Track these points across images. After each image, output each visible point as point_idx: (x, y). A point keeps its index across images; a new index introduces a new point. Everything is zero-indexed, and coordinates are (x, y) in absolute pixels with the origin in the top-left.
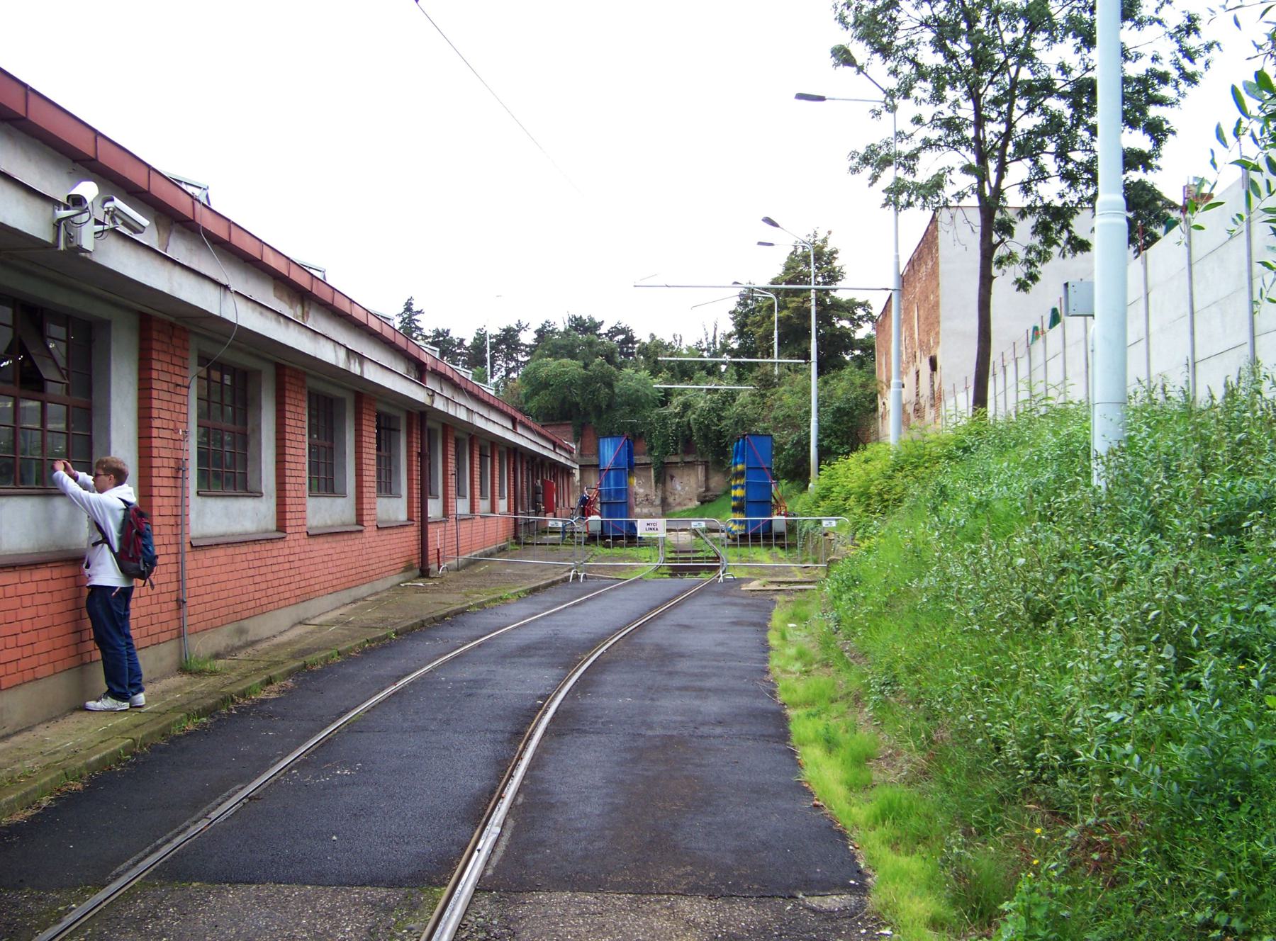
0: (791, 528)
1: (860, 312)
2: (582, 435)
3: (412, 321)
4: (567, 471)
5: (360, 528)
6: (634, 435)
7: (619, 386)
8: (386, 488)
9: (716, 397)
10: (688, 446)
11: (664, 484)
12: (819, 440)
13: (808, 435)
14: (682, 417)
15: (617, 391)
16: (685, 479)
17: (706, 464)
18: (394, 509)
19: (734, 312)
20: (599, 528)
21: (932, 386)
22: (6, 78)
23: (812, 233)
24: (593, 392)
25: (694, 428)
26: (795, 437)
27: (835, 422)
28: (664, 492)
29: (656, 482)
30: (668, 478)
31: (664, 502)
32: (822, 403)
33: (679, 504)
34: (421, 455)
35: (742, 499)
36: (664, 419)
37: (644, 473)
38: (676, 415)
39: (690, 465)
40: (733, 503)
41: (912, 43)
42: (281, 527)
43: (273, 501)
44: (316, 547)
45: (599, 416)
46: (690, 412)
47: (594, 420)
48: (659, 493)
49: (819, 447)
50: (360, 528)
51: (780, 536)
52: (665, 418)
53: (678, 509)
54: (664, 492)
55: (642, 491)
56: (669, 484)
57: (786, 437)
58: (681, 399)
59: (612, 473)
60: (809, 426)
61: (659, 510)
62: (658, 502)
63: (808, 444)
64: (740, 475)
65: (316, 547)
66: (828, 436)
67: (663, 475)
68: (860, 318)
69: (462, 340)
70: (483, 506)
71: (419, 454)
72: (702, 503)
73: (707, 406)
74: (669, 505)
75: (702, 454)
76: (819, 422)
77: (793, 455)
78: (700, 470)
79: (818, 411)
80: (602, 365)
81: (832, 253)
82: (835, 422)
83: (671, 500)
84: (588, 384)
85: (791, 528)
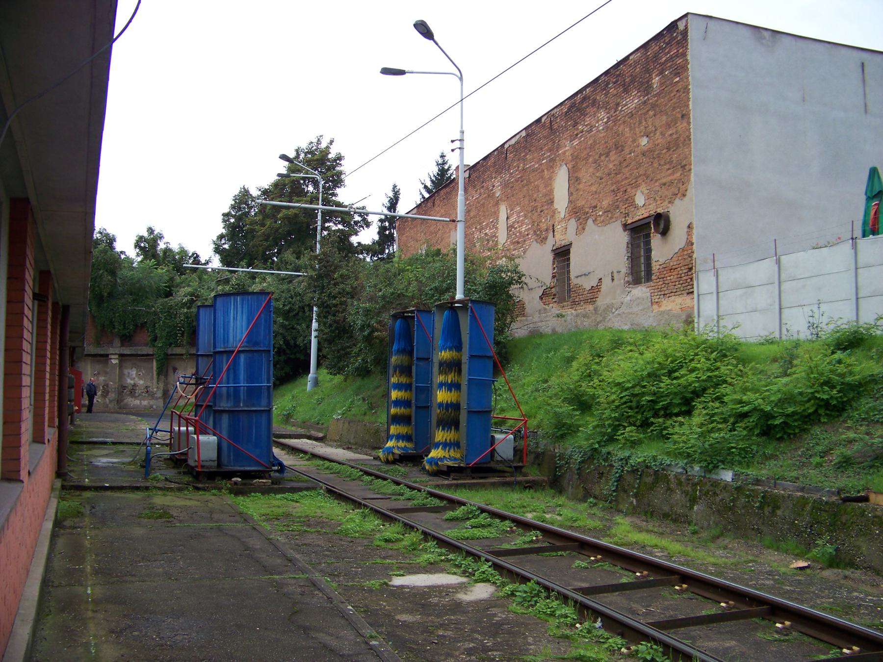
11: (166, 376)
20: (214, 455)
21: (215, 316)
23: (315, 140)
28: (166, 384)
29: (159, 374)
30: (171, 371)
31: (165, 393)
38: (184, 305)
48: (161, 385)
52: (171, 307)
54: (166, 384)
55: (141, 382)
59: (242, 357)
61: (161, 403)
62: (159, 394)
67: (165, 367)
68: (356, 223)
71: (36, 296)
81: (339, 158)
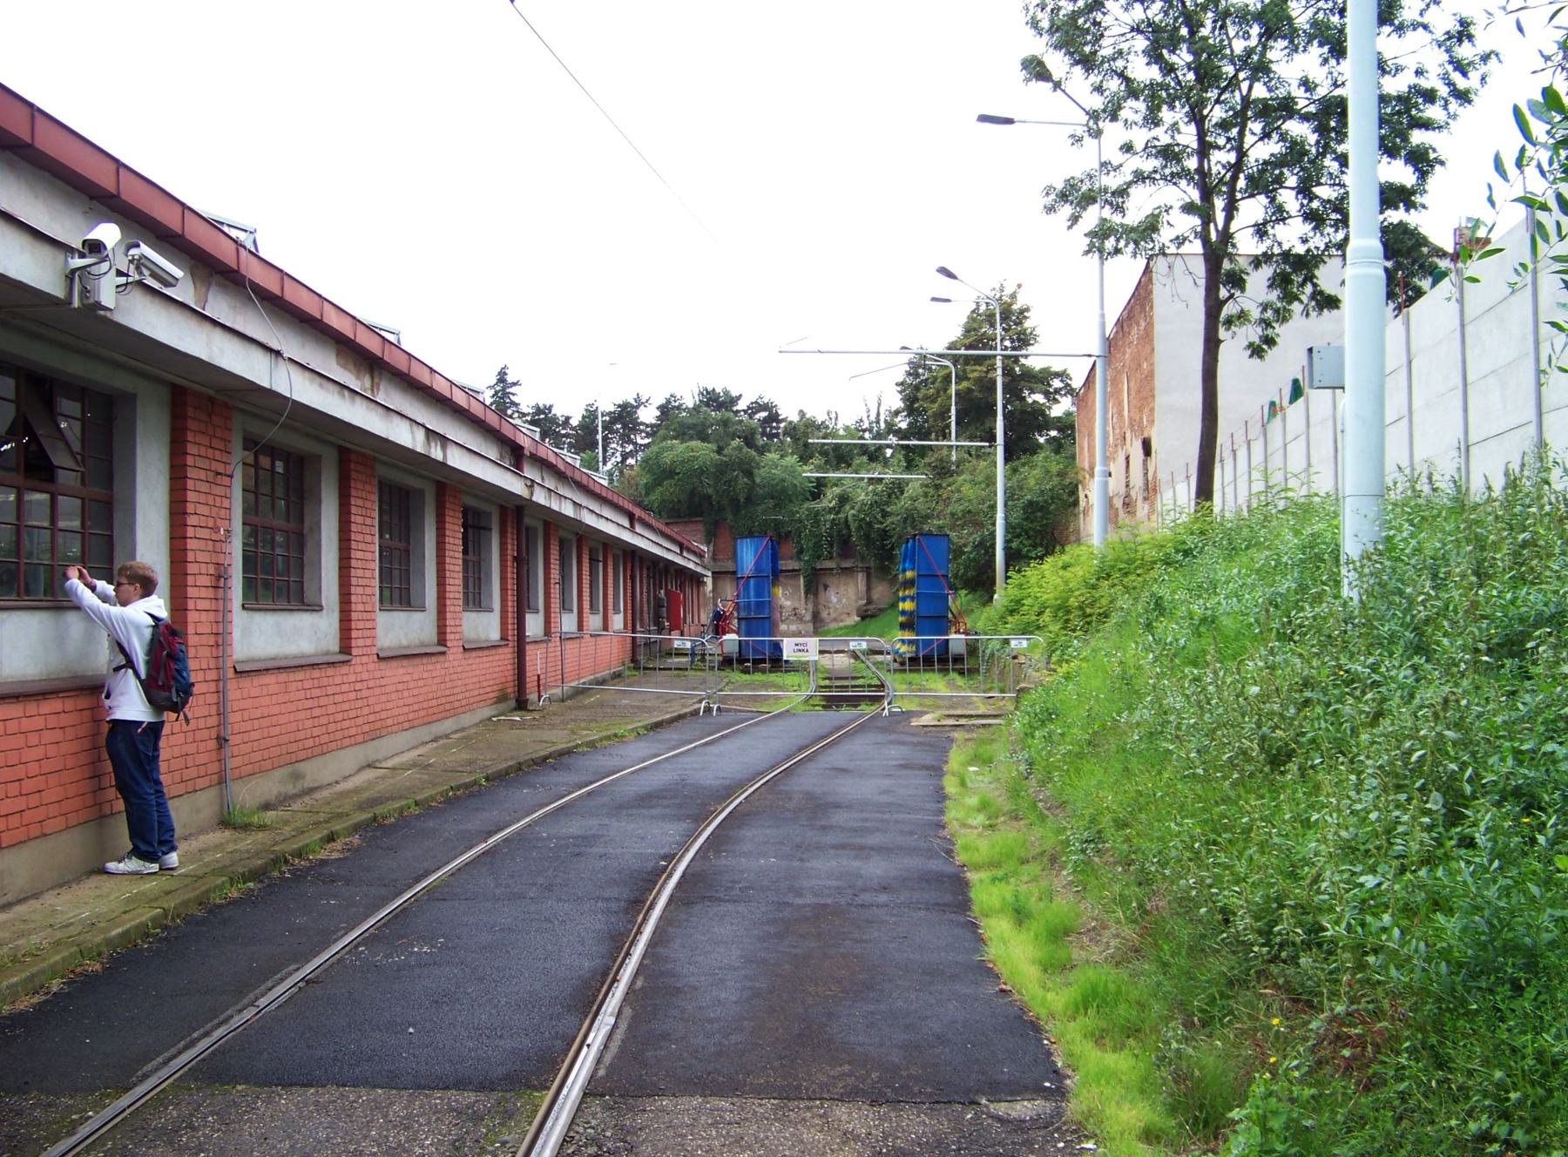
0: (972, 649)
1: (1057, 383)
2: (715, 535)
3: (506, 394)
4: (697, 580)
5: (442, 649)
6: (779, 535)
7: (760, 475)
8: (475, 600)
9: (880, 488)
10: (846, 548)
11: (816, 595)
12: (1007, 542)
13: (993, 535)
14: (838, 513)
15: (758, 480)
16: (842, 589)
17: (867, 570)
18: (485, 625)
19: (902, 384)
20: (737, 649)
22: (7, 96)
23: (998, 287)
24: (728, 482)
25: (853, 527)
26: (977, 537)
27: (1026, 519)
28: (816, 604)
29: (806, 593)
30: (821, 588)
31: (816, 617)
32: (1010, 496)
33: (835, 620)
34: (517, 559)
35: (911, 613)
36: (816, 515)
37: (792, 582)
38: (831, 510)
39: (847, 572)
40: (901, 619)
41: (1120, 53)
42: (346, 648)
43: (336, 616)
44: (388, 673)
45: (736, 511)
46: (848, 507)
47: (730, 517)
48: (810, 606)
49: (1007, 549)
50: (442, 649)
51: (958, 659)
52: (817, 514)
53: (833, 625)
54: (816, 604)
55: (788, 603)
56: (822, 595)
57: (966, 538)
58: (837, 490)
59: (752, 582)
60: (994, 524)
61: (810, 627)
62: (808, 617)
63: (993, 546)
64: (909, 583)
65: (388, 673)
66: (1018, 536)
67: (815, 584)
68: (1057, 391)
69: (568, 419)
70: (594, 622)
72: (863, 618)
73: (868, 499)
74: (822, 621)
75: (863, 559)
76: (1006, 518)
77: (974, 560)
78: (861, 578)
79: (1006, 505)
80: (739, 449)
81: (1022, 311)
82: (1026, 519)
83: (824, 614)
84: (722, 473)
85: (972, 649)
